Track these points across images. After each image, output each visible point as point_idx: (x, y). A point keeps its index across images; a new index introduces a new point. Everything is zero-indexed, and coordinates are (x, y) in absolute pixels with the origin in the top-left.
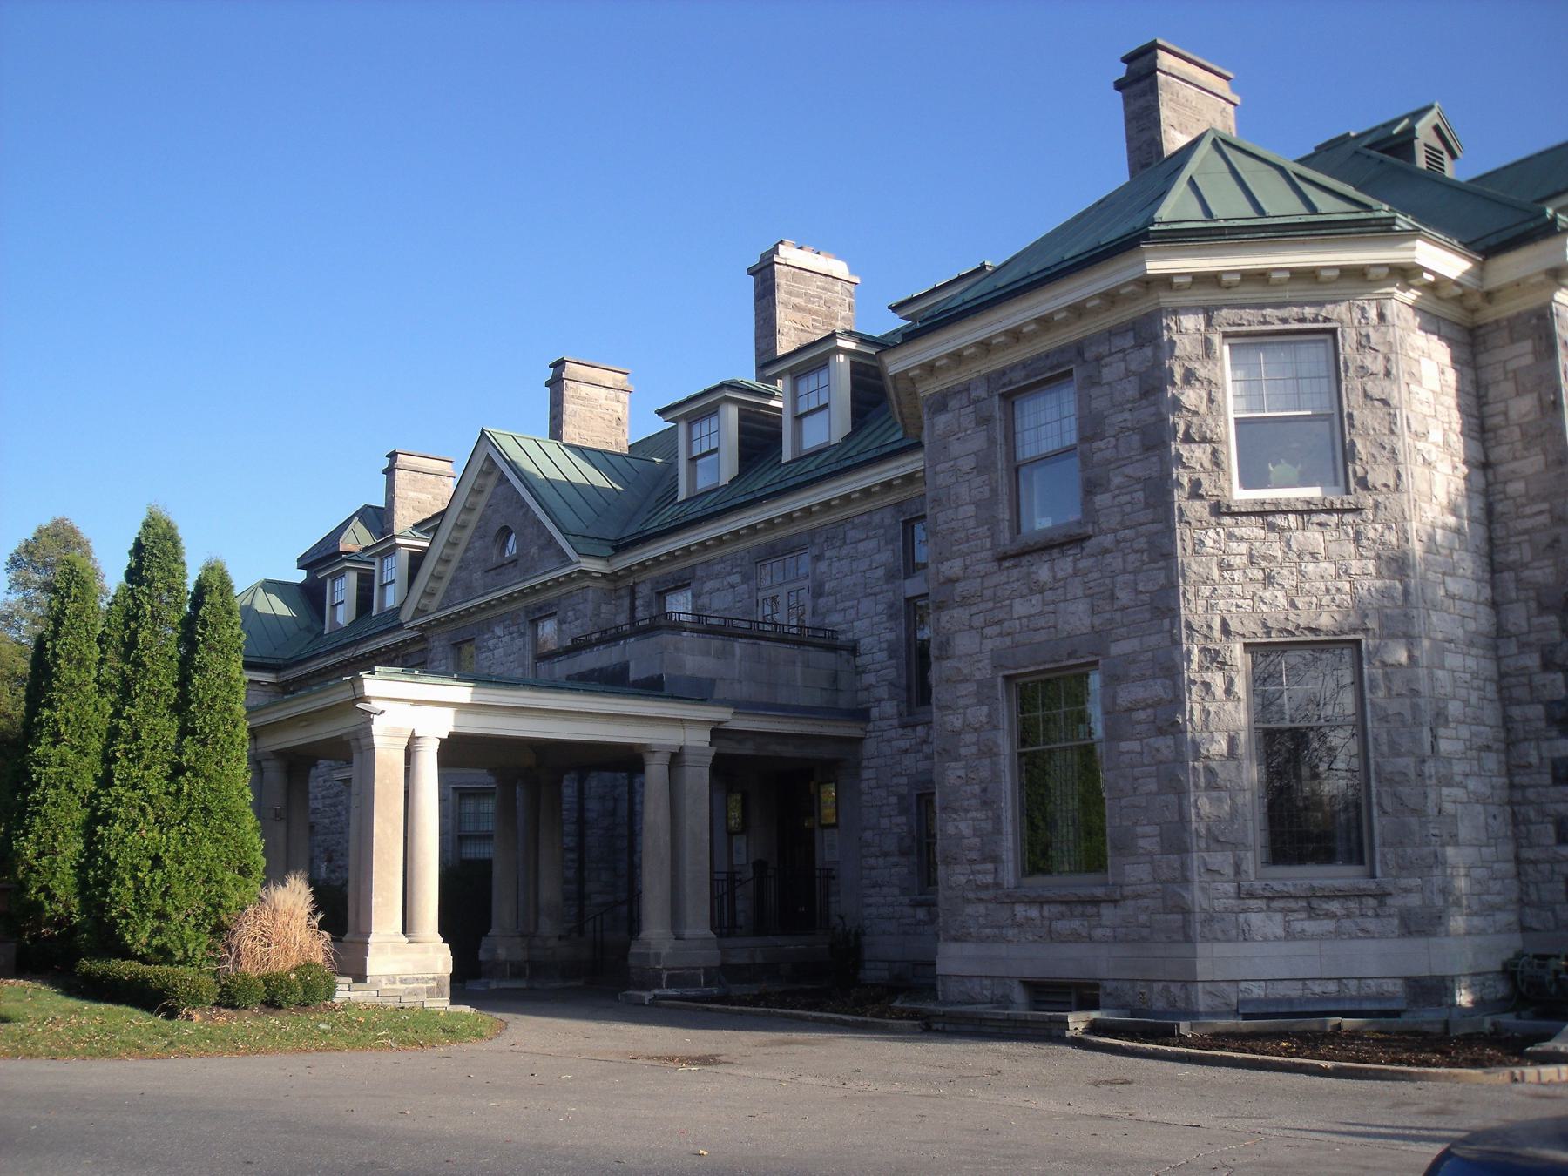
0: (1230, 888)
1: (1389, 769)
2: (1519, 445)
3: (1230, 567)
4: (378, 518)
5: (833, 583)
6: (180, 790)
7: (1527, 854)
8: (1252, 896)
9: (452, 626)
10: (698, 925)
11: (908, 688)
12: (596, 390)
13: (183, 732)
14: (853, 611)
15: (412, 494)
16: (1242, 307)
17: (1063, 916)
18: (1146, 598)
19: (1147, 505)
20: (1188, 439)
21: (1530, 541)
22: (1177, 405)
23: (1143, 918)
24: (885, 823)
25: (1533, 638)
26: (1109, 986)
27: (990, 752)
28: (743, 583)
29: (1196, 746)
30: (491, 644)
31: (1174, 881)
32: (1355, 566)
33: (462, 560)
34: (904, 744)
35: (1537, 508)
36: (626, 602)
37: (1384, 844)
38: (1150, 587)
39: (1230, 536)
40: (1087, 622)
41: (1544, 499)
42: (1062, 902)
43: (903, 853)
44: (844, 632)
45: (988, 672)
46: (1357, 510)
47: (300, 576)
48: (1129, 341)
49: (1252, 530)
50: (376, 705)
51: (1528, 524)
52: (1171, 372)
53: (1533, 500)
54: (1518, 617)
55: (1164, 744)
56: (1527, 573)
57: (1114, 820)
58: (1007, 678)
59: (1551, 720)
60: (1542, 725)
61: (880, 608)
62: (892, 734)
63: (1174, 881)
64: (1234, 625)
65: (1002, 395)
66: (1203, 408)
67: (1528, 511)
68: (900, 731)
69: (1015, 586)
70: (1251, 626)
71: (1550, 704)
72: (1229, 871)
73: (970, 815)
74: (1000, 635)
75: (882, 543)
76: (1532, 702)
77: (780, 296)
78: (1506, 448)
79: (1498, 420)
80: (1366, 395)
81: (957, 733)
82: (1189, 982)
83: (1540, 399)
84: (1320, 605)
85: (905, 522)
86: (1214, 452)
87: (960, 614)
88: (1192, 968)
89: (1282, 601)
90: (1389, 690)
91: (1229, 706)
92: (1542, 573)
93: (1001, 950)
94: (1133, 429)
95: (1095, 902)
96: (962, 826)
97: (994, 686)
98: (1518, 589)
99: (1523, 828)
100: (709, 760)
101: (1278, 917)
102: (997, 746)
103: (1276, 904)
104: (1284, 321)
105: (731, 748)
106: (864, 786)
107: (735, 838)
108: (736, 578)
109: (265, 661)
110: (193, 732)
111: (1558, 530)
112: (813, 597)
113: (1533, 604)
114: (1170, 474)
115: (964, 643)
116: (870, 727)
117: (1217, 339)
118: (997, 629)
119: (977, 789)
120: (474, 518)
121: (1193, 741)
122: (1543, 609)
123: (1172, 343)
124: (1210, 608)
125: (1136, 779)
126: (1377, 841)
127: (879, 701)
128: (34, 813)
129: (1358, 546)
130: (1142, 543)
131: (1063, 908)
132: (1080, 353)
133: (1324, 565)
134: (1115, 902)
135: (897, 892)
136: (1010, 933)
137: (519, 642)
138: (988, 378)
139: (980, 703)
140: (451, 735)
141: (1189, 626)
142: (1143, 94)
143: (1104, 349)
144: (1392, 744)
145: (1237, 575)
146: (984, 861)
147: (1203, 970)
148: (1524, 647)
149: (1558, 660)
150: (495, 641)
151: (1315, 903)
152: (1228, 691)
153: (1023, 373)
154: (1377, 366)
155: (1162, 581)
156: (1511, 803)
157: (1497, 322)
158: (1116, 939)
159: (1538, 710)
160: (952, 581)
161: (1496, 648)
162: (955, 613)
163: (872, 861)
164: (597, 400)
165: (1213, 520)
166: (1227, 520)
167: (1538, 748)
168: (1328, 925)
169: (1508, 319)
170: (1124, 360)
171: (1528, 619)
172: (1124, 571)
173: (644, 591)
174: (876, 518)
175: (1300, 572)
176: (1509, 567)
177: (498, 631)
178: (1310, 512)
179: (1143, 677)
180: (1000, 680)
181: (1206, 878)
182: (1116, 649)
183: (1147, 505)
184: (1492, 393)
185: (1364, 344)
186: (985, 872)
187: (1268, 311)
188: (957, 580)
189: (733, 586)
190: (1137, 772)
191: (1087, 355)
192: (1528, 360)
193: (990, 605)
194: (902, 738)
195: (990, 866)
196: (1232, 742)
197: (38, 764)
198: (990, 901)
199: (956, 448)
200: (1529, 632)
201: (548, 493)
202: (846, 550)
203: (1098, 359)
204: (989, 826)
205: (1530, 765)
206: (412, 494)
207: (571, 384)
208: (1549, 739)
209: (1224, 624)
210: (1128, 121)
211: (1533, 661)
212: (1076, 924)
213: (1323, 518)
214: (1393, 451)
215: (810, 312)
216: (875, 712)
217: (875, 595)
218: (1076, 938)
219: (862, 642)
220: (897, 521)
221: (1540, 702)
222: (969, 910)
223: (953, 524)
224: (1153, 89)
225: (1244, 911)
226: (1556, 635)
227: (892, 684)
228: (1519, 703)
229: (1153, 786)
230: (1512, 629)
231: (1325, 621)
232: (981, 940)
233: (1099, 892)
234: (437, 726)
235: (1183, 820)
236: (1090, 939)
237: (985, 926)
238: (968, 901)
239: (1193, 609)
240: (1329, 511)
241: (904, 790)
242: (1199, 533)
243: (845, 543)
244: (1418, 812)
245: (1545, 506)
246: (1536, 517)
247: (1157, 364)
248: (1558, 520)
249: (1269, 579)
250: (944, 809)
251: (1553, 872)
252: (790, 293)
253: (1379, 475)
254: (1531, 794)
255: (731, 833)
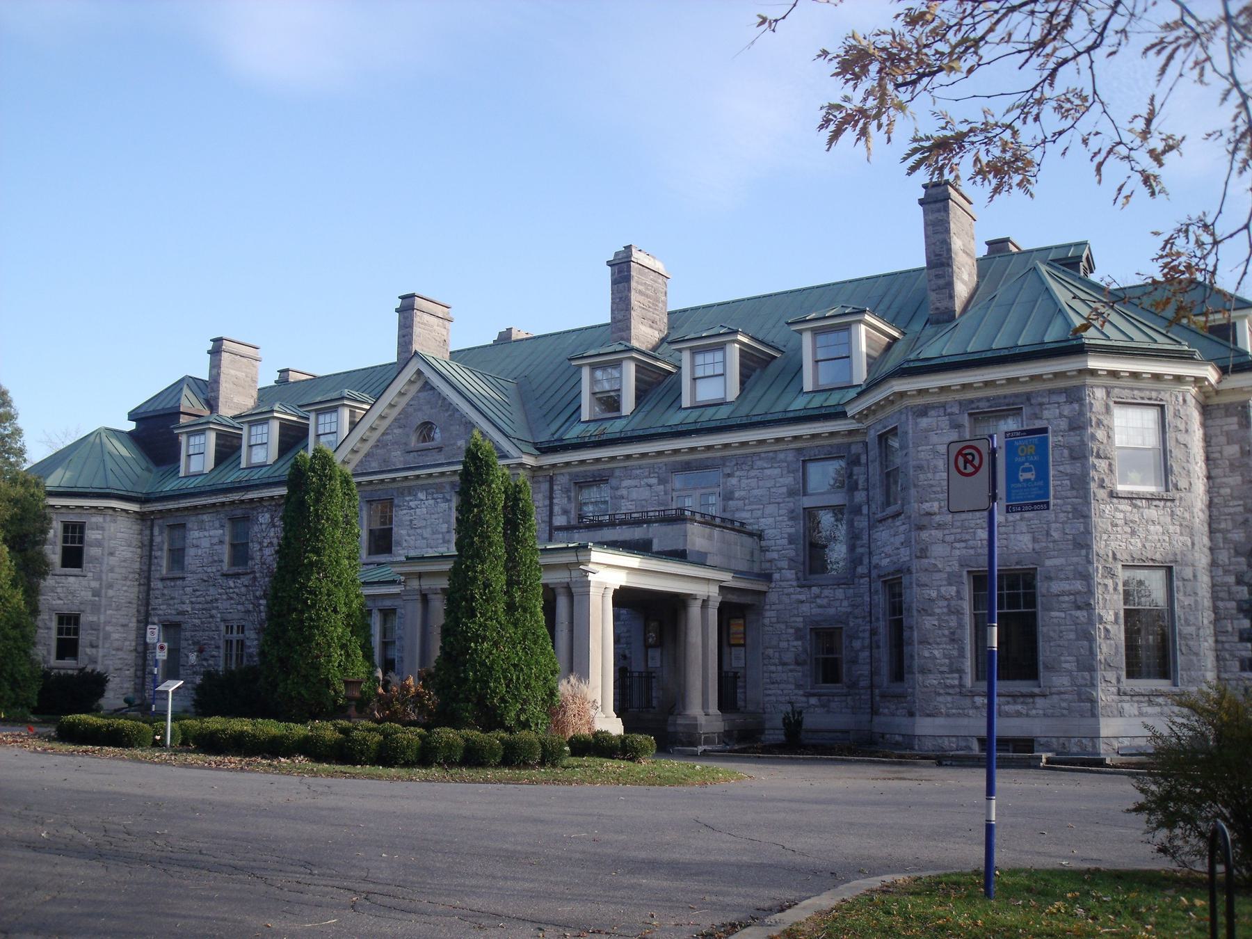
0: (1114, 690)
1: (1185, 632)
2: (1227, 470)
3: (1116, 525)
4: (208, 391)
5: (743, 493)
6: (518, 619)
7: (1224, 675)
8: (1125, 694)
9: (369, 488)
10: (714, 709)
11: (804, 563)
12: (432, 318)
13: (510, 583)
14: (759, 513)
15: (233, 372)
16: (1124, 388)
17: (1008, 703)
18: (1070, 537)
19: (1072, 488)
20: (1098, 456)
21: (1232, 519)
22: (1093, 437)
23: (1064, 705)
24: (784, 645)
25: (1231, 568)
26: (1043, 740)
27: (958, 613)
28: (659, 484)
29: (1101, 617)
30: (412, 504)
31: (1086, 685)
32: (1171, 529)
33: (378, 441)
34: (803, 597)
35: (1236, 503)
36: (545, 486)
37: (1182, 670)
38: (1073, 532)
39: (1116, 509)
40: (1030, 546)
41: (1241, 499)
42: (1009, 696)
43: (797, 663)
44: (751, 524)
45: (956, 567)
46: (1173, 500)
47: (132, 426)
48: (1062, 399)
49: (1125, 506)
50: (591, 567)
51: (1232, 510)
52: (1091, 420)
53: (1233, 498)
54: (1223, 557)
55: (1081, 615)
56: (1229, 535)
57: (1045, 652)
58: (969, 572)
59: (1240, 609)
60: (1234, 612)
61: (782, 512)
62: (792, 590)
63: (1086, 685)
64: (1119, 556)
65: (970, 415)
66: (1105, 441)
67: (1231, 504)
68: (799, 589)
69: (978, 521)
70: (1126, 556)
71: (1239, 602)
72: (1114, 681)
73: (941, 646)
74: (966, 548)
75: (785, 472)
76: (1230, 600)
77: (633, 284)
78: (1220, 470)
79: (1217, 455)
80: (1177, 440)
81: (931, 600)
82: (1095, 737)
83: (1241, 448)
84: (1155, 548)
85: (804, 461)
86: (1110, 465)
87: (938, 534)
88: (1098, 730)
89: (1139, 545)
90: (1185, 593)
91: (1115, 597)
92: (1238, 536)
93: (965, 721)
94: (1064, 446)
95: (1033, 695)
96: (936, 652)
97: (961, 576)
98: (1224, 543)
99: (1221, 663)
100: (718, 605)
101: (1136, 705)
102: (963, 609)
103: (1135, 699)
104: (1142, 398)
105: (733, 598)
106: (767, 621)
107: (649, 650)
108: (654, 481)
109: (130, 494)
110: (518, 583)
111: (1248, 515)
112: (723, 500)
113: (1232, 551)
114: (1089, 474)
115: (938, 550)
116: (773, 585)
117: (1111, 404)
118: (963, 545)
119: (946, 632)
120: (394, 413)
121: (1099, 614)
122: (1237, 553)
123: (1091, 404)
124: (1106, 546)
125: (1061, 632)
126: (1179, 668)
127: (781, 569)
128: (311, 627)
129: (1172, 519)
130: (1069, 508)
131: (1010, 699)
132: (1029, 399)
133: (1158, 527)
134: (1044, 696)
135: (793, 687)
136: (971, 712)
137: (444, 506)
138: (960, 403)
139: (950, 584)
140: (621, 587)
141: (1098, 555)
142: (939, 211)
143: (1046, 400)
144: (1186, 620)
145: (1119, 529)
146: (951, 672)
147: (1104, 732)
148: (1226, 572)
149: (1246, 580)
150: (416, 503)
151: (1152, 698)
152: (1115, 589)
153: (987, 404)
154: (1182, 427)
155: (1082, 529)
156: (1216, 650)
157: (1218, 405)
158: (1045, 715)
159: (1234, 604)
160: (929, 514)
161: (1211, 571)
162: (933, 532)
163: (773, 668)
164: (432, 326)
165: (1108, 500)
166: (1115, 500)
167: (1232, 623)
168: (1158, 709)
169: (1225, 405)
170: (1059, 407)
171: (1229, 559)
172: (1056, 522)
173: (562, 480)
174: (781, 456)
175: (1147, 530)
176: (1219, 531)
177: (421, 495)
178: (1152, 499)
179: (1067, 579)
180: (965, 573)
181: (1104, 684)
182: (1048, 563)
183: (1072, 488)
184: (1214, 441)
185: (1177, 415)
186: (952, 679)
187: (1136, 392)
188: (935, 514)
189: (650, 486)
190: (1063, 628)
191: (1033, 401)
192: (1236, 427)
193: (959, 530)
194: (800, 593)
195: (956, 675)
196: (1116, 615)
197: (310, 593)
198: (955, 694)
199: (934, 439)
200: (1230, 565)
201: (575, 391)
202: (753, 473)
203: (1041, 404)
204: (955, 653)
205: (1227, 632)
206: (233, 372)
207: (418, 313)
208: (1238, 619)
209: (1114, 554)
210: (926, 225)
211: (1231, 579)
212: (1019, 707)
213: (1157, 503)
214: (1189, 471)
215: (647, 296)
216: (776, 576)
217: (779, 503)
218: (1018, 714)
219: (766, 532)
220: (798, 460)
221: (1234, 600)
222: (940, 699)
223: (931, 482)
224: (946, 209)
225: (1121, 701)
226: (1245, 568)
227: (791, 560)
228: (1222, 600)
229: (1072, 636)
230: (1221, 563)
231: (1158, 557)
232: (948, 715)
233: (1036, 690)
234: (620, 579)
235: (1092, 653)
236: (1027, 715)
237: (952, 708)
238: (939, 694)
239: (1099, 546)
240: (1160, 500)
241: (801, 625)
242: (1102, 506)
243: (752, 468)
244: (1197, 654)
245: (1241, 502)
246: (1236, 507)
247: (1081, 413)
248: (1249, 510)
249: (1133, 533)
250: (920, 643)
251: (1238, 685)
252: (637, 282)
253: (1183, 484)
254: (1227, 646)
255: (647, 647)
